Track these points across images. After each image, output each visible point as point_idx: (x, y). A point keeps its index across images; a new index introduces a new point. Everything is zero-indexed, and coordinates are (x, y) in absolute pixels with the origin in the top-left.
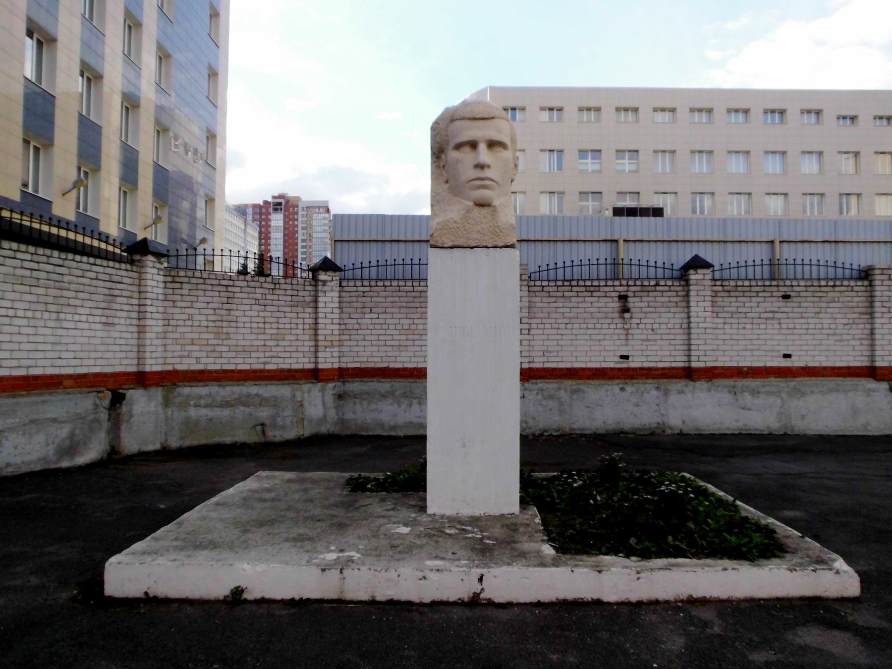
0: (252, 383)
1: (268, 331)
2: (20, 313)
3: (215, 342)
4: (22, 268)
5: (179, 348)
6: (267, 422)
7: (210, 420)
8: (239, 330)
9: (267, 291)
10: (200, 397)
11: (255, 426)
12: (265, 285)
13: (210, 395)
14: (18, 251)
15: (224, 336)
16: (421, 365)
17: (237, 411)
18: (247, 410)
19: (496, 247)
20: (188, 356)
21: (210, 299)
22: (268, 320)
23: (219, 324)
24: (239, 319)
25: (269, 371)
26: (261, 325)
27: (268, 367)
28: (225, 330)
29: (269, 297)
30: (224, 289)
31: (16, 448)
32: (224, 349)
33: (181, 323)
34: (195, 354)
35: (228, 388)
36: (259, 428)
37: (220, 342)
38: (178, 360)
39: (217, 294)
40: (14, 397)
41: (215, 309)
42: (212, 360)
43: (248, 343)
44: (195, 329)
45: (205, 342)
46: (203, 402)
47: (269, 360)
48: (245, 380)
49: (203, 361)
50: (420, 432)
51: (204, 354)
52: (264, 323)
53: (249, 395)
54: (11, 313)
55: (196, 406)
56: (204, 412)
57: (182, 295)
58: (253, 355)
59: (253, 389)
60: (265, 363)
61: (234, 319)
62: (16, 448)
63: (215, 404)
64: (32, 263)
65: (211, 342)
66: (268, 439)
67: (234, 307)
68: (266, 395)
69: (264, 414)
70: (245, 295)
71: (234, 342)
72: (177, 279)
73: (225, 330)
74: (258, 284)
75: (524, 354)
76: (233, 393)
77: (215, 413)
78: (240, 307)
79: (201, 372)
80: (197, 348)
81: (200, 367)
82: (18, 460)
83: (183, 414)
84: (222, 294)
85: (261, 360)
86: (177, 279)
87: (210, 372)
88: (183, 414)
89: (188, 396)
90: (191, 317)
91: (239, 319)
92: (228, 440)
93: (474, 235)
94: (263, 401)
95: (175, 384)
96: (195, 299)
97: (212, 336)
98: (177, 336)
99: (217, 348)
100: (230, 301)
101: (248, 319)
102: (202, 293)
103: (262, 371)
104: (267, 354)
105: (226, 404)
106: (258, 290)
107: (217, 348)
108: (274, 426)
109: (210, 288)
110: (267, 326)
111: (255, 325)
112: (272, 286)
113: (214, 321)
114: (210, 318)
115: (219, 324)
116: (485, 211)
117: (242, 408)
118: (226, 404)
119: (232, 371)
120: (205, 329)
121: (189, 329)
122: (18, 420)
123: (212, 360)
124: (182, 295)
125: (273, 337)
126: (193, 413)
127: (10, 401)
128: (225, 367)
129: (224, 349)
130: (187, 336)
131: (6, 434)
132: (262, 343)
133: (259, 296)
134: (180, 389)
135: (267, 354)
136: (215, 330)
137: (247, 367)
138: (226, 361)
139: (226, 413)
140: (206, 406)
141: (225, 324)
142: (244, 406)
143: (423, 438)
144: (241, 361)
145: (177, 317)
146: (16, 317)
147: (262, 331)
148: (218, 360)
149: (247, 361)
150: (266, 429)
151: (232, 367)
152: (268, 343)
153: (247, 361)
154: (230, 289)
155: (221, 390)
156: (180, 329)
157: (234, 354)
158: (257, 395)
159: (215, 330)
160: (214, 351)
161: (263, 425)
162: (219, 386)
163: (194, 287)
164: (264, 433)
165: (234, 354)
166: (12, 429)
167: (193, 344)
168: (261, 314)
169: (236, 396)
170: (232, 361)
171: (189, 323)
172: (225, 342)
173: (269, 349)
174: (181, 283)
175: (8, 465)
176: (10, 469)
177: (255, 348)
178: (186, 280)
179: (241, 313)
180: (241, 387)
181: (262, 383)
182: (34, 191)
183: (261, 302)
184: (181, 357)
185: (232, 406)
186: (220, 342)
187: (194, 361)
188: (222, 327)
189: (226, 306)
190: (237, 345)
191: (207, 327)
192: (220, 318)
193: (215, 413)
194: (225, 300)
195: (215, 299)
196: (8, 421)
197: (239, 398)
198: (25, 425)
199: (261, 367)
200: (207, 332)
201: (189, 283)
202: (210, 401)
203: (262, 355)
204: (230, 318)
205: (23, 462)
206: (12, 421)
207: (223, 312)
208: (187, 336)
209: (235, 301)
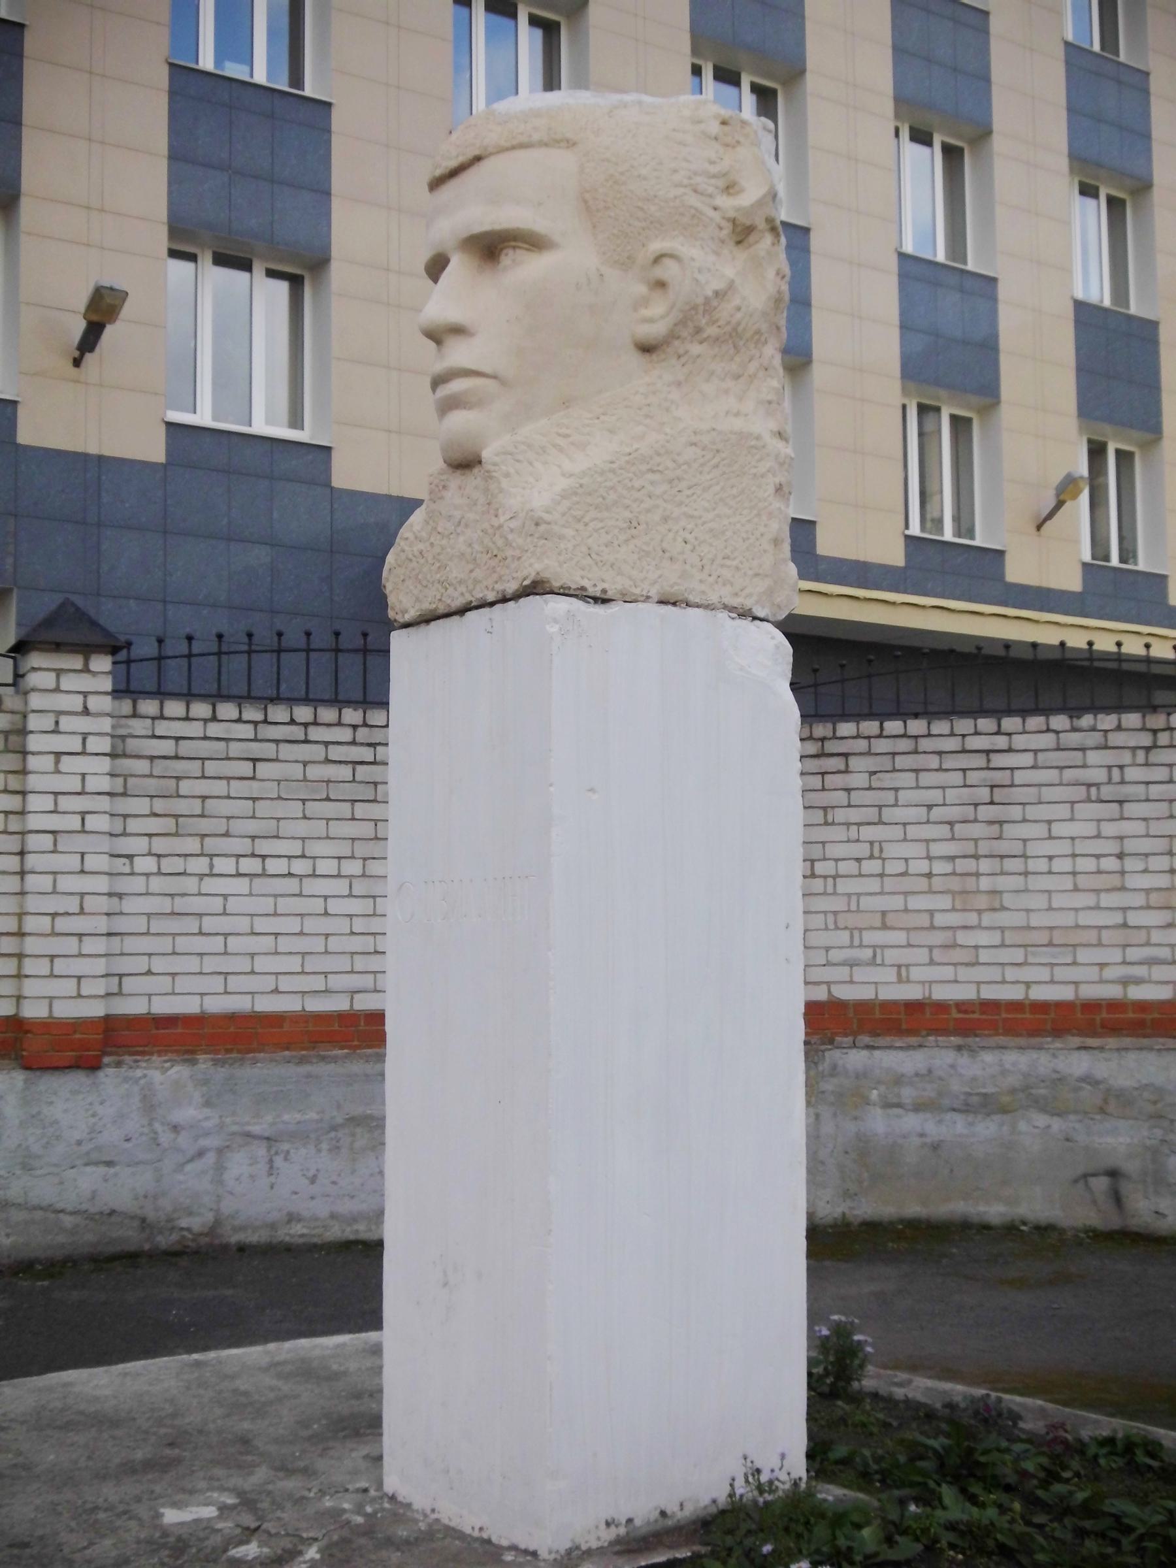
0: (1076, 1041)
1: (1133, 881)
2: (324, 867)
3: (954, 919)
4: (328, 761)
5: (844, 937)
6: (1131, 1167)
7: (936, 1147)
8: (1035, 883)
9: (1126, 757)
10: (899, 1080)
11: (1085, 1176)
12: (1116, 739)
13: (929, 1074)
14: (315, 723)
15: (982, 902)
16: (365, 1003)
17: (1022, 1126)
18: (1057, 1124)
19: (504, 600)
20: (873, 962)
21: (935, 796)
22: (1131, 846)
23: (969, 865)
24: (1032, 849)
25: (1143, 1006)
26: (1110, 864)
27: (1137, 993)
28: (985, 883)
29: (1132, 774)
30: (980, 761)
31: (313, 1180)
32: (983, 938)
33: (844, 868)
34: (891, 956)
35: (988, 1057)
36: (1101, 1184)
37: (972, 918)
38: (843, 973)
39: (957, 778)
40: (302, 1061)
41: (951, 824)
42: (948, 972)
43: (1067, 919)
44: (889, 884)
45: (924, 920)
46: (907, 1094)
47: (1140, 971)
48: (1058, 1032)
49: (916, 973)
50: (362, 1231)
51: (922, 955)
52: (1120, 856)
53: (1059, 1080)
54: (300, 867)
55: (887, 1105)
56: (911, 1122)
57: (848, 790)
58: (1083, 956)
59: (1074, 1061)
60: (1125, 982)
61: (1017, 848)
62: (313, 1180)
63: (946, 1102)
64: (353, 749)
65: (940, 919)
66: (1134, 1224)
67: (1015, 812)
68: (1123, 1081)
69: (1119, 1140)
70: (1051, 775)
71: (1018, 919)
72: (831, 747)
73: (985, 883)
74: (1094, 739)
75: (818, 974)
76: (1004, 1073)
77: (953, 1128)
78: (1032, 812)
79: (914, 1007)
80: (899, 937)
81: (912, 993)
82: (321, 1209)
83: (851, 1127)
84: (973, 778)
85: (1110, 973)
86: (831, 747)
87: (941, 1007)
88: (851, 1127)
89: (862, 1075)
90: (876, 851)
91: (1032, 849)
92: (995, 1212)
93: (456, 572)
94: (1112, 1102)
95: (831, 1042)
96: (889, 797)
97: (945, 902)
98: (839, 904)
99: (962, 938)
100: (999, 795)
101: (1064, 847)
102: (908, 779)
103: (1114, 1006)
104: (1134, 954)
105: (983, 1104)
106: (1093, 757)
107: (962, 938)
108: (1158, 1180)
109: (934, 762)
110: (1130, 864)
111: (1088, 864)
112: (1146, 740)
113: (952, 858)
114: (937, 849)
115: (969, 865)
116: (472, 480)
117: (1041, 1120)
118: (983, 1104)
119: (1015, 1006)
120: (923, 884)
121: (874, 885)
122: (312, 1115)
123: (948, 972)
124: (848, 790)
125: (1154, 899)
126: (878, 1123)
127: (294, 1071)
128: (989, 993)
129: (983, 938)
130: (866, 903)
131: (285, 1146)
132: (1118, 918)
133: (1100, 775)
134: (837, 1054)
135: (1134, 954)
136: (955, 884)
137: (1064, 994)
138: (994, 974)
139: (987, 1129)
140: (918, 1108)
141: (985, 866)
142: (1044, 1110)
143: (373, 1250)
144: (1043, 974)
145: (834, 851)
146: (314, 875)
147: (1115, 880)
148: (964, 973)
149: (1061, 973)
150: (1126, 1188)
151: (1014, 993)
152: (1134, 919)
153: (1061, 973)
154: (998, 760)
155: (963, 1060)
156: (843, 886)
157: (1018, 955)
158: (1087, 1079)
159: (955, 884)
160: (954, 946)
161: (1113, 1174)
162: (959, 1048)
163: (886, 763)
164: (1117, 1198)
165: (1018, 955)
166: (299, 1135)
167: (885, 927)
168: (1109, 829)
169: (1013, 1081)
170: (1011, 974)
171: (872, 866)
172: (987, 919)
173: (1141, 937)
174: (846, 755)
175: (292, 1218)
176: (298, 1229)
177: (1092, 937)
178: (862, 745)
179: (1040, 830)
180: (1034, 1055)
181: (1112, 1042)
182: (958, 533)
183: (1107, 792)
184: (852, 964)
185: (1004, 1110)
186: (972, 918)
187: (890, 975)
188: (977, 875)
189: (985, 812)
190: (1029, 928)
191: (929, 875)
192: (969, 848)
193: (953, 1128)
194: (984, 794)
195: (951, 795)
196: (286, 1117)
197: (1026, 1088)
198: (334, 1128)
199: (1113, 992)
200: (931, 891)
201: (869, 753)
202: (930, 1091)
203: (1115, 955)
204: (1003, 847)
205: (333, 1216)
206: (298, 1116)
207: (977, 830)
208: (866, 903)
209: (1018, 794)
